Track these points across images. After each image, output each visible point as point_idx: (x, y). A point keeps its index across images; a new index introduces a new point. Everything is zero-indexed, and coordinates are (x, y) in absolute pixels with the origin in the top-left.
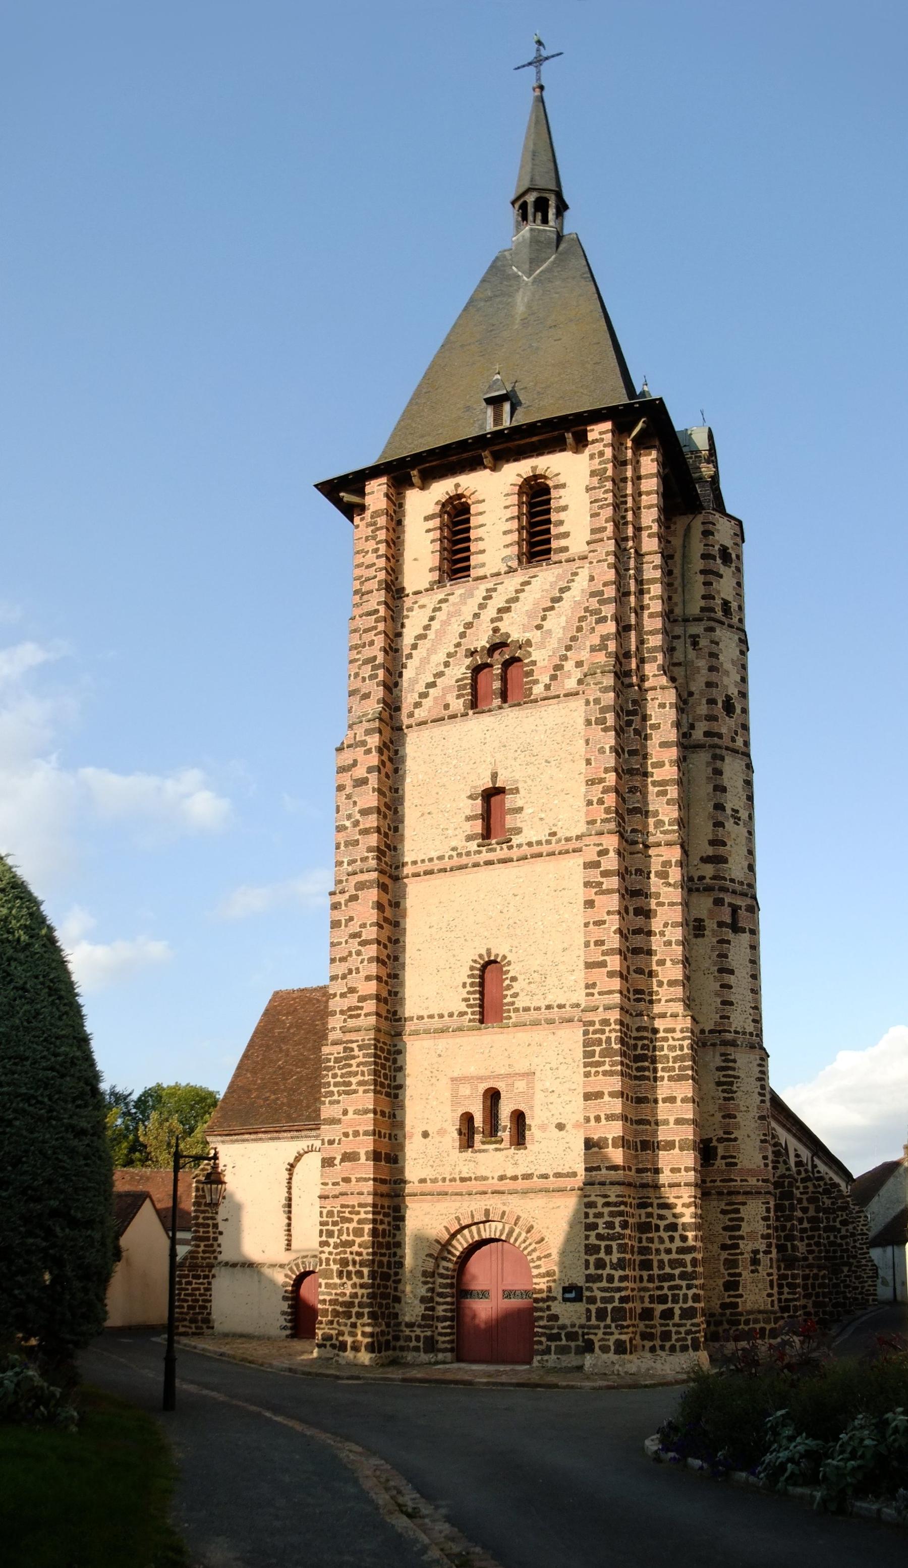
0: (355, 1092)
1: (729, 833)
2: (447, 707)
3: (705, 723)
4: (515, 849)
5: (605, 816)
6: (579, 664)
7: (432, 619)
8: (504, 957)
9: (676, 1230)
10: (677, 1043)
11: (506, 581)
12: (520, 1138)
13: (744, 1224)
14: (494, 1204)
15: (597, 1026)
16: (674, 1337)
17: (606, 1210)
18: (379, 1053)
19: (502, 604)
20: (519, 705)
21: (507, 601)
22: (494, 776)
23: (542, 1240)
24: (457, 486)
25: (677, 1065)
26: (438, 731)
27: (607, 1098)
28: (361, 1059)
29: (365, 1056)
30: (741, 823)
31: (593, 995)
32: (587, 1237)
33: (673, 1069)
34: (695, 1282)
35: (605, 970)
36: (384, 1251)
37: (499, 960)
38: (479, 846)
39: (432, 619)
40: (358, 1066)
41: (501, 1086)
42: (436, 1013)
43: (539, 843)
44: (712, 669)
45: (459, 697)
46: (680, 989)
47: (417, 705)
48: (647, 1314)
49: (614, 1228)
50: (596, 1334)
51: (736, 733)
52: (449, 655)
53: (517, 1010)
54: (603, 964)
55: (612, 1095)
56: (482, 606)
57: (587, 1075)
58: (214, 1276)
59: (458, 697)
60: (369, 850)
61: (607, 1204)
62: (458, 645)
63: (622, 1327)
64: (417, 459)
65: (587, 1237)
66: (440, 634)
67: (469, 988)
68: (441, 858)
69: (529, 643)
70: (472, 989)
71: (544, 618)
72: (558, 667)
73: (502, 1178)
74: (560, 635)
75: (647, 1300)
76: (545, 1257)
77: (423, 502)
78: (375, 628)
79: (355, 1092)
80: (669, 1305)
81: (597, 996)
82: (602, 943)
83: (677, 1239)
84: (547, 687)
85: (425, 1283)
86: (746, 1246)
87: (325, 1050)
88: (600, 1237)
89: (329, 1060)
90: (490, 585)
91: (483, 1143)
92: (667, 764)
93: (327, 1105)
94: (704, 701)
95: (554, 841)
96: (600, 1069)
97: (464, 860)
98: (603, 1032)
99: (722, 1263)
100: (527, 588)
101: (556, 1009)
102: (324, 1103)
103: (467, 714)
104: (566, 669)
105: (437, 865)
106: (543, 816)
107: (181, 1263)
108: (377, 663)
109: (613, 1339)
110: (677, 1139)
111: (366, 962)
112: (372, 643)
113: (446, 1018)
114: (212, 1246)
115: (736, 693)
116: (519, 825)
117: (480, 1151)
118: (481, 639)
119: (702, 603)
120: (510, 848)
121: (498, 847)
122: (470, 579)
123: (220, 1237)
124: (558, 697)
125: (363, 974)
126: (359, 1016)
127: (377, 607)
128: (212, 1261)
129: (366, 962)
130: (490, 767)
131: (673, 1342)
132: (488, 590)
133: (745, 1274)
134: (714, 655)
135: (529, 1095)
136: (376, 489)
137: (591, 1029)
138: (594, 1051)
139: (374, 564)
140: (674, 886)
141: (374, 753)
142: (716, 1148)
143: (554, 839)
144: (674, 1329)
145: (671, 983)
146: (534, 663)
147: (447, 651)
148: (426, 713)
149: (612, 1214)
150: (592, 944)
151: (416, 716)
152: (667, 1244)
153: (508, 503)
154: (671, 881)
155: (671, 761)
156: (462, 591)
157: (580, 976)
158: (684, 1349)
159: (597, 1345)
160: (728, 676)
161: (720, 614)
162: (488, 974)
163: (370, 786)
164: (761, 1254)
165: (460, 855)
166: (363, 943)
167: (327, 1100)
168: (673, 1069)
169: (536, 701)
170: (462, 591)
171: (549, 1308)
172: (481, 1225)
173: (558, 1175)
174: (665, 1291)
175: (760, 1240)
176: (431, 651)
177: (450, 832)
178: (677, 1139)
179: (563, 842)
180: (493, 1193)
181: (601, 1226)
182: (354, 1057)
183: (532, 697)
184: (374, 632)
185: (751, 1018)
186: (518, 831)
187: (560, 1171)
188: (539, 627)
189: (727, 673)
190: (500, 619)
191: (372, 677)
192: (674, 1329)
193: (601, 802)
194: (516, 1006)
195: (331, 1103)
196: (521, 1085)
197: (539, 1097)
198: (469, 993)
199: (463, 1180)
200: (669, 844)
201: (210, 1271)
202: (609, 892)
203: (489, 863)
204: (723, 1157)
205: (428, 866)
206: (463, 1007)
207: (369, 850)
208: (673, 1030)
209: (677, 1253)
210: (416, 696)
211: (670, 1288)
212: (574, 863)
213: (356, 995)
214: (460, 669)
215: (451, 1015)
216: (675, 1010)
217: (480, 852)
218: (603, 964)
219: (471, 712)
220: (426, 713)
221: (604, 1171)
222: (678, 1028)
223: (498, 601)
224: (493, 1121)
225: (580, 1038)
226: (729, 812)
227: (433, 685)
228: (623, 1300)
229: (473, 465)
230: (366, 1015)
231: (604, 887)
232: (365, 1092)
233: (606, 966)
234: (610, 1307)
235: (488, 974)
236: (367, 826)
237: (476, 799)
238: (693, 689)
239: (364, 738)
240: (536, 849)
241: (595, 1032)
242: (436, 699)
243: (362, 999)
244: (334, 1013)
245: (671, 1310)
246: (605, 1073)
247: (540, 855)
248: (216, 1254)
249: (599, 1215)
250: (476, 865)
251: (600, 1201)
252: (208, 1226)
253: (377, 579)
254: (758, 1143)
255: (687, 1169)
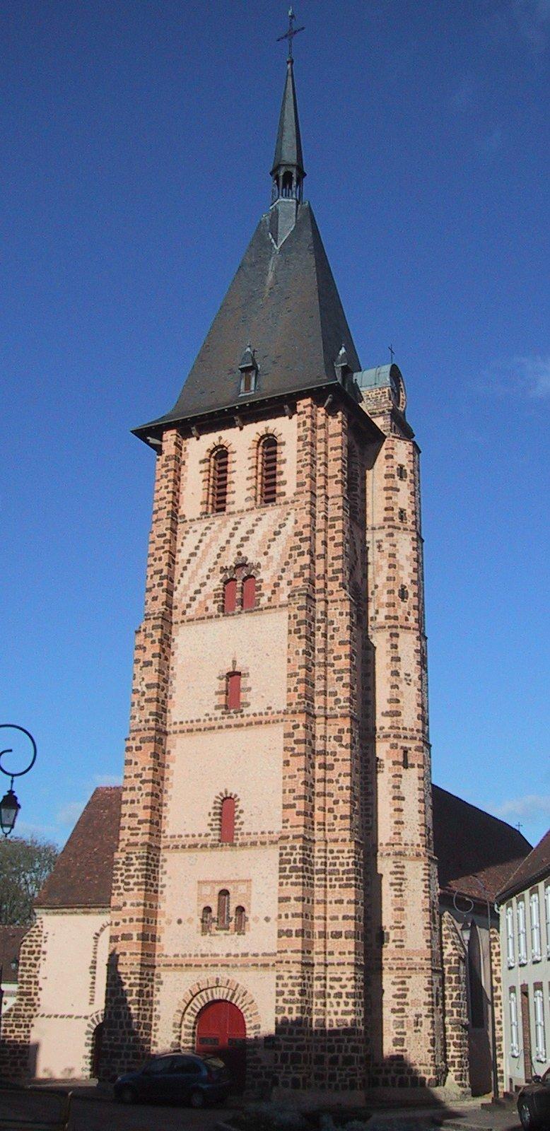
0: (132, 889)
1: (402, 693)
2: (207, 609)
3: (386, 609)
4: (245, 718)
5: (298, 700)
6: (289, 583)
7: (200, 541)
8: (236, 796)
9: (341, 997)
10: (345, 861)
11: (247, 517)
12: (240, 929)
13: (409, 994)
14: (223, 974)
15: (288, 850)
16: (338, 1078)
17: (290, 982)
18: (150, 862)
19: (244, 535)
20: (251, 612)
21: (248, 533)
22: (234, 662)
23: (253, 1001)
24: (220, 438)
25: (345, 877)
26: (201, 627)
27: (293, 902)
28: (137, 866)
29: (140, 864)
30: (412, 683)
31: (286, 827)
32: (277, 1001)
33: (342, 879)
34: (352, 1037)
35: (294, 810)
36: (146, 1007)
37: (233, 797)
38: (223, 714)
39: (200, 541)
40: (135, 871)
41: (230, 888)
42: (190, 834)
43: (261, 714)
44: (392, 566)
45: (215, 602)
46: (348, 821)
47: (189, 606)
48: (320, 1060)
49: (294, 995)
50: (280, 1073)
51: (409, 614)
52: (210, 570)
53: (242, 834)
54: (293, 806)
55: (297, 899)
56: (232, 535)
57: (281, 884)
58: (32, 1026)
59: (215, 602)
60: (151, 714)
61: (291, 977)
62: (216, 563)
63: (297, 1068)
64: (194, 420)
65: (277, 1001)
66: (205, 554)
67: (212, 817)
68: (198, 721)
69: (259, 566)
70: (214, 818)
71: (269, 547)
72: (276, 585)
73: (228, 955)
74: (278, 561)
75: (319, 1049)
76: (255, 1014)
77: (198, 447)
78: (163, 547)
79: (132, 889)
80: (336, 1054)
81: (289, 829)
82: (294, 791)
83: (342, 1005)
84: (270, 599)
85: (174, 1032)
86: (411, 1012)
87: (117, 855)
88: (285, 1001)
89: (118, 863)
90: (237, 519)
91: (217, 929)
92: (343, 657)
93: (116, 896)
94: (385, 592)
95: (270, 714)
96: (290, 881)
97: (213, 723)
98: (292, 854)
99: (391, 1023)
100: (259, 523)
101: (267, 835)
102: (114, 894)
103: (219, 616)
104: (281, 586)
105: (196, 725)
106: (264, 695)
107: (6, 1014)
108: (163, 574)
109: (291, 1076)
110: (344, 931)
111: (144, 796)
112: (160, 559)
113: (197, 837)
114: (32, 1000)
115: (409, 583)
116: (248, 700)
117: (215, 935)
118: (230, 561)
119: (385, 514)
120: (242, 716)
121: (234, 715)
122: (225, 513)
123: (40, 993)
124: (275, 607)
125: (141, 805)
126: (138, 834)
127: (165, 532)
128: (32, 1012)
129: (144, 796)
130: (232, 656)
131: (337, 1082)
132: (236, 523)
133: (409, 1033)
134: (393, 556)
135: (248, 896)
136: (169, 437)
137: (284, 852)
138: (286, 868)
139: (165, 498)
140: (346, 747)
141: (157, 643)
142: (388, 934)
143: (270, 712)
144: (338, 1072)
145: (342, 817)
146: (261, 581)
147: (208, 567)
148: (194, 613)
149: (293, 985)
150: (287, 791)
151: (187, 614)
152: (336, 1008)
153: (250, 455)
154: (344, 744)
155: (345, 655)
156: (220, 522)
157: (279, 812)
158: (345, 1087)
159: (281, 1080)
160: (403, 570)
161: (397, 520)
162: (226, 808)
163: (153, 667)
164: (423, 1017)
165: (210, 719)
166: (143, 782)
167: (116, 892)
168: (342, 879)
169: (261, 609)
170: (220, 522)
171: (255, 1053)
172: (214, 990)
173: (265, 954)
174: (333, 1043)
175: (423, 1006)
176: (199, 566)
177: (205, 702)
178: (344, 931)
179: (276, 714)
180: (222, 966)
181: (286, 993)
182: (132, 865)
183: (260, 607)
184: (162, 551)
185: (418, 833)
186: (248, 705)
187: (266, 951)
188: (266, 554)
189: (402, 568)
190: (242, 546)
191: (160, 585)
192: (338, 1072)
193: (296, 689)
194: (242, 831)
195: (118, 894)
196: (242, 888)
197: (254, 900)
198: (213, 820)
199: (203, 956)
200: (343, 716)
201: (30, 1021)
202: (299, 755)
203: (229, 726)
204: (394, 941)
205: (190, 726)
206: (208, 830)
207: (151, 714)
208: (343, 851)
209: (342, 1014)
210: (188, 598)
211: (337, 1041)
212: (280, 730)
213: (137, 819)
214: (215, 583)
215: (200, 835)
216: (344, 837)
217: (223, 718)
218: (293, 806)
219: (221, 614)
220: (194, 613)
221: (289, 954)
222: (346, 850)
223: (241, 533)
224: (224, 913)
225: (277, 859)
226: (402, 676)
227: (198, 592)
228: (299, 1048)
229: (229, 424)
230: (143, 834)
231: (296, 751)
232: (139, 890)
233: (295, 807)
234: (290, 1052)
235: (226, 808)
236: (150, 696)
237: (221, 679)
238: (378, 583)
239: (151, 631)
240: (258, 718)
241: (287, 854)
242: (200, 602)
243: (140, 822)
244: (124, 828)
245: (337, 1058)
246: (292, 884)
247: (260, 723)
248: (36, 1007)
249: (285, 985)
250: (220, 727)
251: (286, 975)
252: (31, 983)
253: (166, 510)
254: (423, 929)
255: (350, 953)
